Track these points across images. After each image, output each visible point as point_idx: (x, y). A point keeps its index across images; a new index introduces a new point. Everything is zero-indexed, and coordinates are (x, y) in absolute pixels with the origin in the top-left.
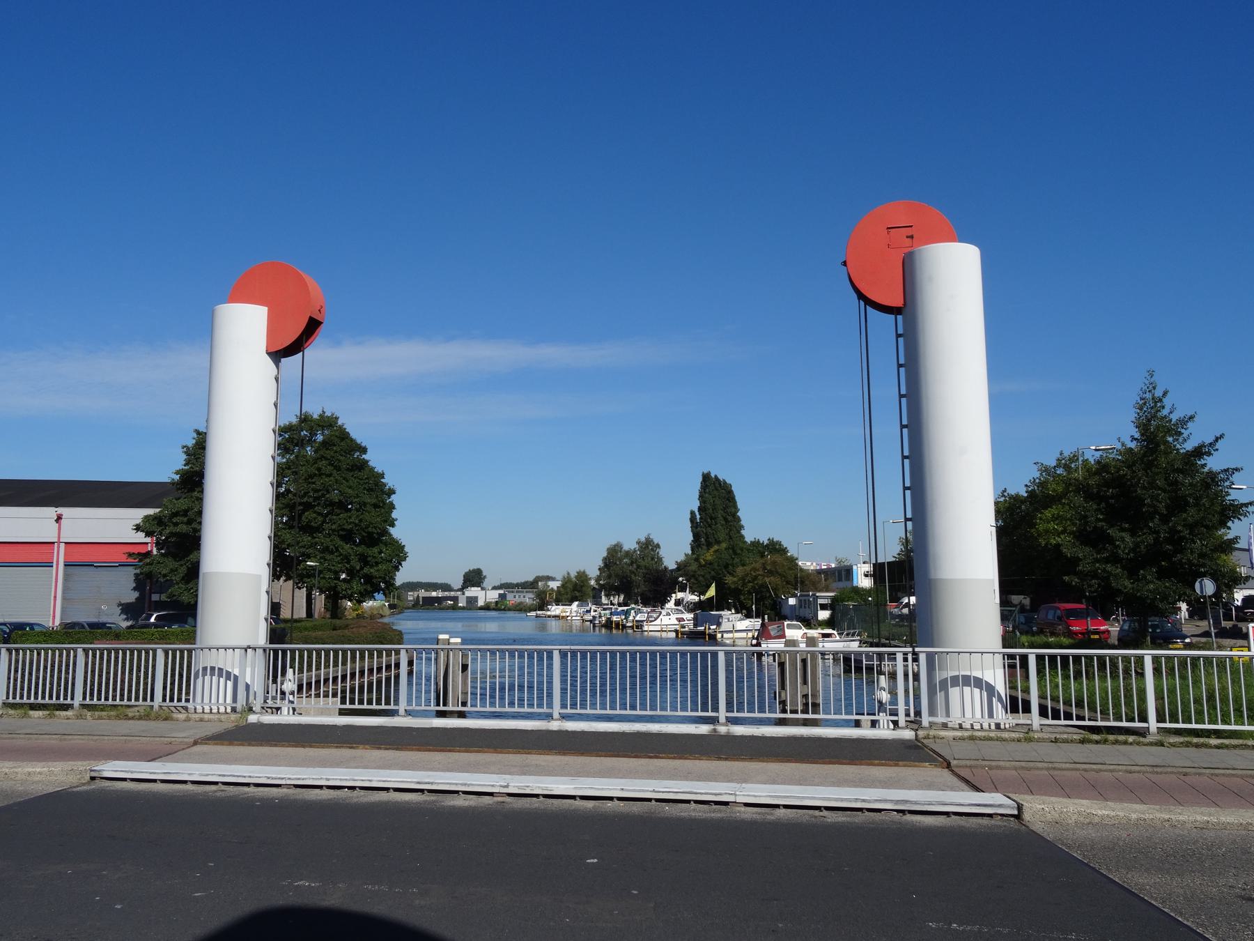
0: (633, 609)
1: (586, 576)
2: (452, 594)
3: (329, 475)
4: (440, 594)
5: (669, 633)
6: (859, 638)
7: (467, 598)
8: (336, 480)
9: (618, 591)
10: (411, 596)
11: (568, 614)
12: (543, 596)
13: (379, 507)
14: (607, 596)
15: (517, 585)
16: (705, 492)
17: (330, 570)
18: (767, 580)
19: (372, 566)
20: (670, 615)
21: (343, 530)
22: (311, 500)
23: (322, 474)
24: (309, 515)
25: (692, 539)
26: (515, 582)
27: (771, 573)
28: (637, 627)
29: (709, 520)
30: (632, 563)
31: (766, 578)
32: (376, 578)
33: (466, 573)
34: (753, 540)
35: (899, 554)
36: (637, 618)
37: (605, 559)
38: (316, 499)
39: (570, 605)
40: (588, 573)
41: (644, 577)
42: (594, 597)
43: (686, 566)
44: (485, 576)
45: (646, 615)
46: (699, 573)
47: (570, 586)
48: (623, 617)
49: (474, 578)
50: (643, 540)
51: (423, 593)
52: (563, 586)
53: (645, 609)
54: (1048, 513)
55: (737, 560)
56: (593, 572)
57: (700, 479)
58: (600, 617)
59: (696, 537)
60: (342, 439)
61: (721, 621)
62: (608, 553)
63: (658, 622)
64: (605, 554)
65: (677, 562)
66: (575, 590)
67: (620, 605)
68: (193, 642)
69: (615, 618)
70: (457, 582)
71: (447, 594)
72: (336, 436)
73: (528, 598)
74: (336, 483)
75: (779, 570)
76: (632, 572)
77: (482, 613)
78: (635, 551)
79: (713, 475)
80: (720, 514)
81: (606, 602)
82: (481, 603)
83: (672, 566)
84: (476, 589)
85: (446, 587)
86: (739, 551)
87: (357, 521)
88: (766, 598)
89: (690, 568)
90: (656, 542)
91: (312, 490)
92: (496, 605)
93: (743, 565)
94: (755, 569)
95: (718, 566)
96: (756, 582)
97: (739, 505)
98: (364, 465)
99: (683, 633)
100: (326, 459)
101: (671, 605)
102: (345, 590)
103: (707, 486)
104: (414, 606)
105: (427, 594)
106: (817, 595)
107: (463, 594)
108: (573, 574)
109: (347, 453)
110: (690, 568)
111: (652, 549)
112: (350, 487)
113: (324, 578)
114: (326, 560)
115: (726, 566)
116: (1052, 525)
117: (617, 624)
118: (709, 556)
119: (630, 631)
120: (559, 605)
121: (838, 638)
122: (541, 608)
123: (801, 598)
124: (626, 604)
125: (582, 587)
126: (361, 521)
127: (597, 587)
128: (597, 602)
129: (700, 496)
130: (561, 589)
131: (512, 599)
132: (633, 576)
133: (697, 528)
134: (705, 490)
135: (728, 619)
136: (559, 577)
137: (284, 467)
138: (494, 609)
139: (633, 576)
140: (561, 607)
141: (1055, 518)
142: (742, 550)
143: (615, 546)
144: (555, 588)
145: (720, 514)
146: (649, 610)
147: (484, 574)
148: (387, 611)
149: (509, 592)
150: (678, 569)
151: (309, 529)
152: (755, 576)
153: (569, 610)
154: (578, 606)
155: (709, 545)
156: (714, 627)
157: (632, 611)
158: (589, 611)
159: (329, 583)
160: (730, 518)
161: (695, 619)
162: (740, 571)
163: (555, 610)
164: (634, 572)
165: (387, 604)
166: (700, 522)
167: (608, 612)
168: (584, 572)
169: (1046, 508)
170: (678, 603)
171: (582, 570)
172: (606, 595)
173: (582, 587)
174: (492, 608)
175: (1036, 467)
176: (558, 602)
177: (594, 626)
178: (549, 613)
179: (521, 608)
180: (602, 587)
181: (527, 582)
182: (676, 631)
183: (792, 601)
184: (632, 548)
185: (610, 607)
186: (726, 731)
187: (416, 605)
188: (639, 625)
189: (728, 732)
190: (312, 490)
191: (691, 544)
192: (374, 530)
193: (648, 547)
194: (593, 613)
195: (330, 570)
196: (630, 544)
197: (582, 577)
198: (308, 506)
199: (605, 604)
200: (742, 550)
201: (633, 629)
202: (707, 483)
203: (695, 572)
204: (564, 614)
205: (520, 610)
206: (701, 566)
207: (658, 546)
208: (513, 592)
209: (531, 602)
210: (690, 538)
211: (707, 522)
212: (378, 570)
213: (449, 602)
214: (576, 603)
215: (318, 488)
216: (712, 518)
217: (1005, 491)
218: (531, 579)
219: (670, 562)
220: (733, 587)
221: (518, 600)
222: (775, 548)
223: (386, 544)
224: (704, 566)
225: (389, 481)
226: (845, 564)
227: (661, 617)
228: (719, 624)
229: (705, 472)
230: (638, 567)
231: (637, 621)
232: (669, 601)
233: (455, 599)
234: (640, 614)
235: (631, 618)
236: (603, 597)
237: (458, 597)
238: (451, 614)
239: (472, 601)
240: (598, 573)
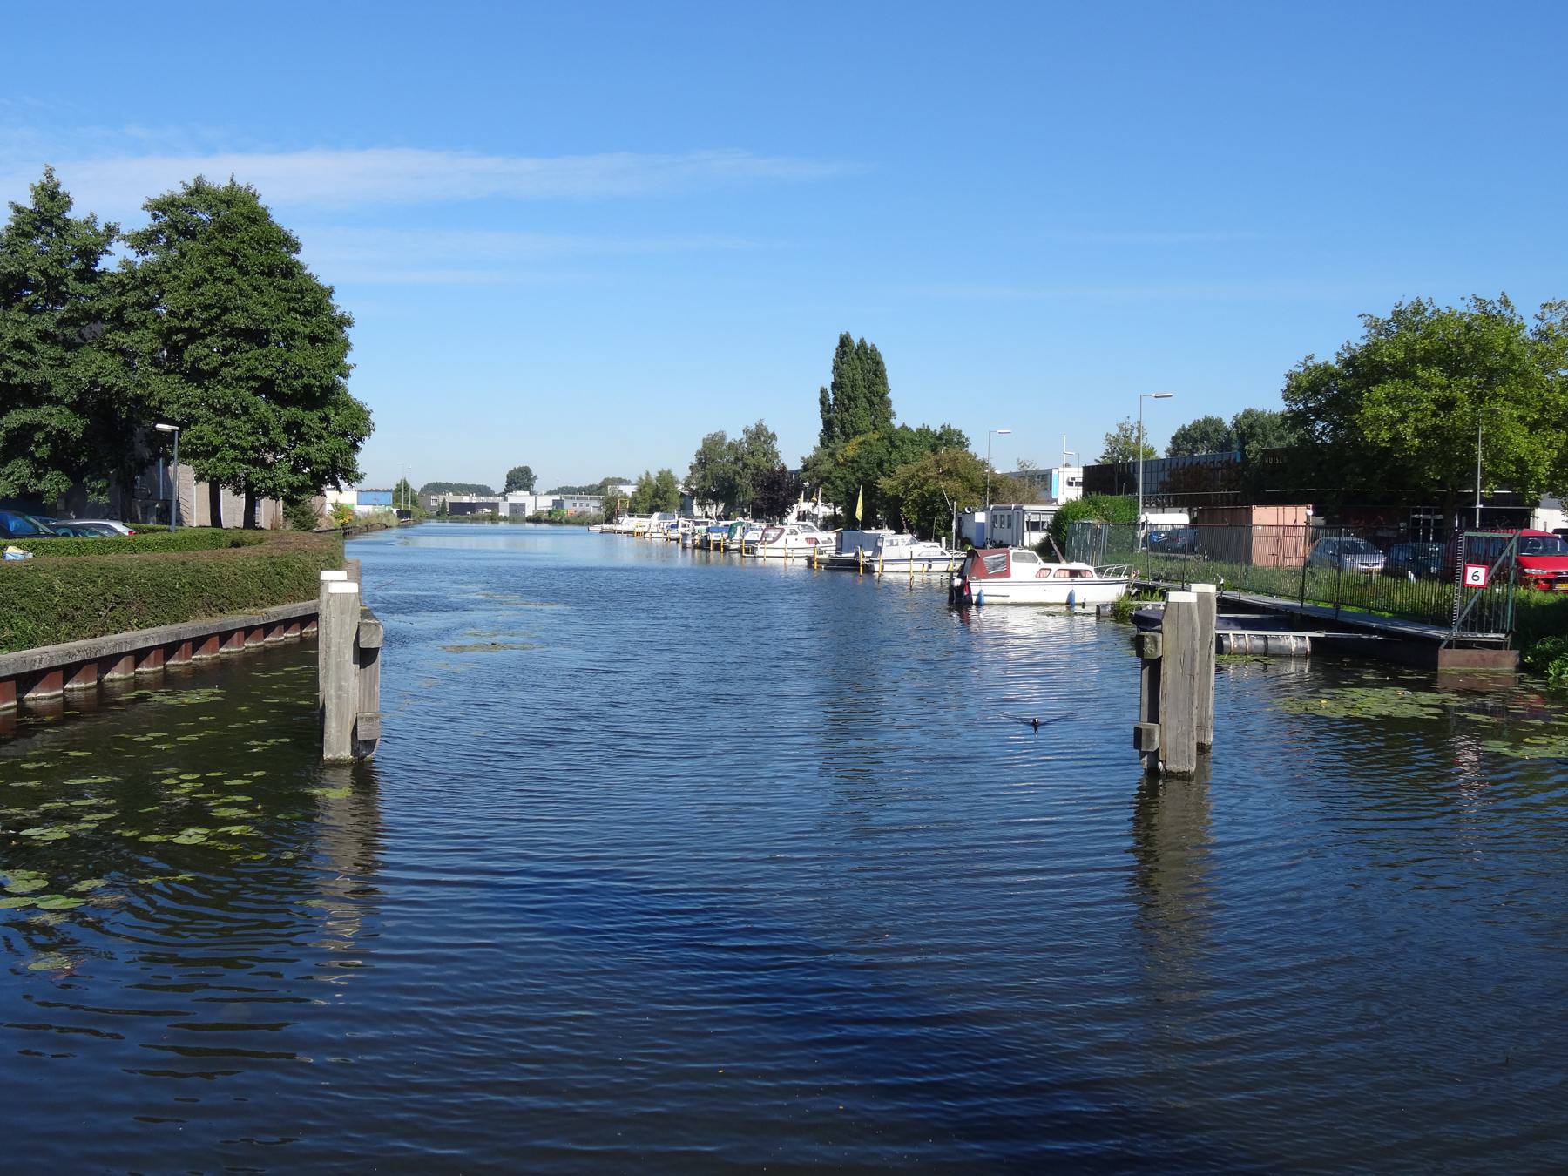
0: (741, 523)
1: (672, 477)
2: (491, 499)
3: (229, 282)
4: (474, 499)
5: (796, 560)
6: (1126, 578)
7: (511, 505)
8: (240, 290)
9: (716, 498)
10: (435, 501)
11: (645, 530)
12: (613, 504)
13: (323, 341)
14: (701, 505)
15: (580, 490)
16: (842, 362)
17: (233, 447)
18: (942, 485)
19: (309, 443)
20: (797, 534)
21: (255, 378)
22: (197, 324)
23: (217, 279)
24: (195, 350)
25: (822, 428)
26: (577, 486)
27: (948, 473)
28: (747, 550)
29: (846, 402)
30: (737, 459)
31: (941, 483)
32: (317, 463)
33: (511, 473)
34: (920, 426)
35: (1103, 457)
36: (747, 538)
37: (699, 454)
38: (210, 321)
39: (649, 517)
40: (674, 473)
41: (754, 480)
42: (682, 507)
43: (816, 465)
44: (535, 477)
45: (760, 533)
46: (835, 474)
47: (650, 491)
48: (726, 535)
49: (520, 479)
50: (753, 427)
51: (451, 498)
52: (639, 490)
53: (757, 525)
54: (1378, 392)
55: (895, 455)
56: (681, 472)
57: (837, 343)
58: (694, 534)
59: (828, 425)
60: (254, 221)
61: (879, 544)
62: (704, 446)
63: (780, 543)
64: (699, 446)
65: (803, 458)
66: (656, 497)
67: (719, 518)
68: (1043, 495)
69: (713, 537)
70: (499, 484)
71: (483, 499)
72: (242, 215)
73: (592, 507)
74: (241, 295)
75: (962, 472)
76: (736, 473)
77: (530, 525)
78: (741, 443)
79: (856, 342)
80: (861, 392)
81: (699, 514)
82: (529, 512)
83: (798, 466)
84: (522, 493)
85: (483, 490)
86: (898, 443)
87: (278, 364)
88: (939, 510)
89: (822, 468)
90: (770, 431)
91: (199, 305)
92: (550, 516)
93: (905, 463)
94: (924, 469)
95: (868, 463)
96: (925, 488)
97: (891, 382)
98: (291, 270)
99: (820, 562)
100: (225, 253)
101: (791, 518)
102: (263, 481)
103: (845, 353)
104: (438, 514)
105: (457, 499)
106: (1025, 508)
107: (506, 499)
108: (654, 475)
109: (261, 245)
110: (822, 468)
111: (765, 442)
112: (265, 304)
113: (223, 459)
114: (225, 428)
115: (880, 464)
116: (1386, 410)
117: (717, 547)
118: (850, 449)
119: (737, 555)
120: (633, 516)
121: (1095, 578)
122: (609, 520)
123: (995, 513)
124: (727, 518)
125: (666, 492)
126: (285, 362)
127: (686, 493)
128: (686, 510)
129: (834, 368)
130: (638, 495)
131: (571, 507)
132: (737, 478)
133: (829, 412)
134: (841, 359)
135: (892, 542)
136: (634, 480)
137: (158, 269)
138: (546, 521)
139: (737, 478)
140: (636, 520)
141: (1391, 400)
142: (903, 442)
143: (715, 435)
144: (630, 495)
145: (861, 392)
146: (764, 525)
147: (534, 473)
148: (394, 521)
149: (566, 498)
150: (805, 468)
151: (196, 376)
152: (924, 479)
153: (647, 525)
154: (660, 518)
155: (847, 437)
156: (869, 553)
157: (739, 528)
158: (674, 526)
159: (233, 468)
160: (876, 400)
161: (840, 540)
162: (901, 471)
163: (628, 523)
164: (739, 473)
165: (395, 511)
166: (834, 404)
167: (703, 527)
168: (669, 472)
169: (1376, 382)
170: (802, 517)
171: (666, 469)
172: (699, 504)
173: (666, 492)
174: (543, 519)
175: (1361, 322)
176: (632, 512)
177: (684, 547)
178: (618, 527)
179: (581, 520)
180: (694, 493)
181: (592, 486)
182: (810, 560)
183: (980, 517)
184: (738, 439)
185: (706, 520)
187: (441, 514)
188: (749, 549)
190: (199, 305)
191: (820, 436)
192: (312, 381)
193: (760, 437)
194: (681, 529)
195: (233, 447)
196: (735, 434)
197: (666, 479)
198: (193, 335)
199: (697, 517)
200: (903, 442)
201: (741, 552)
202: (846, 349)
203: (830, 473)
204: (640, 530)
205: (581, 524)
206: (837, 464)
207: (773, 437)
208: (572, 498)
209: (597, 512)
210: (819, 425)
211: (844, 405)
212: (319, 450)
213: (487, 510)
214: (657, 515)
215: (208, 302)
216: (850, 399)
217: (1310, 357)
218: (598, 482)
219: (793, 463)
220: (890, 493)
221: (578, 509)
222: (950, 439)
223: (335, 405)
224: (843, 464)
225: (341, 304)
226: (1030, 468)
227: (784, 536)
228: (878, 550)
229: (844, 333)
230: (745, 466)
231: (747, 542)
232: (789, 514)
233: (495, 506)
234: (755, 531)
235: (737, 537)
236: (695, 507)
237: (497, 504)
238: (488, 525)
239: (517, 509)
240: (689, 473)
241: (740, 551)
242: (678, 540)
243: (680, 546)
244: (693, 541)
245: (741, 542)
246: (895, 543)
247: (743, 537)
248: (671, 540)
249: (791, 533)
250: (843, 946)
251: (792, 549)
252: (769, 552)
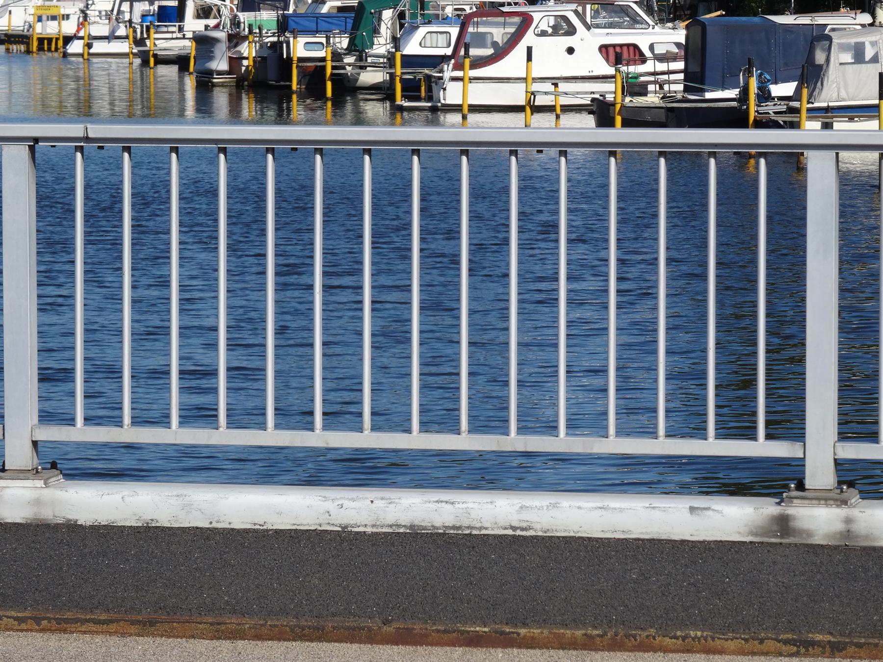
11: (69, 27)
20: (571, 31)
28: (411, 89)
36: (412, 47)
48: (343, 42)
58: (235, 39)
61: (820, 57)
177: (205, 85)
186: (839, 527)
189: (848, 534)
194: (193, 24)
201: (391, 97)
204: (51, 29)
227: (529, 39)
231: (410, 61)
235: (381, 46)
241: (384, 92)
242: (182, 62)
243: (190, 83)
244: (235, 62)
245: (391, 59)
246: (869, 54)
247: (397, 48)
248: (161, 61)
249: (556, 31)
250: (282, 408)
251: (555, 81)
252: (480, 94)
